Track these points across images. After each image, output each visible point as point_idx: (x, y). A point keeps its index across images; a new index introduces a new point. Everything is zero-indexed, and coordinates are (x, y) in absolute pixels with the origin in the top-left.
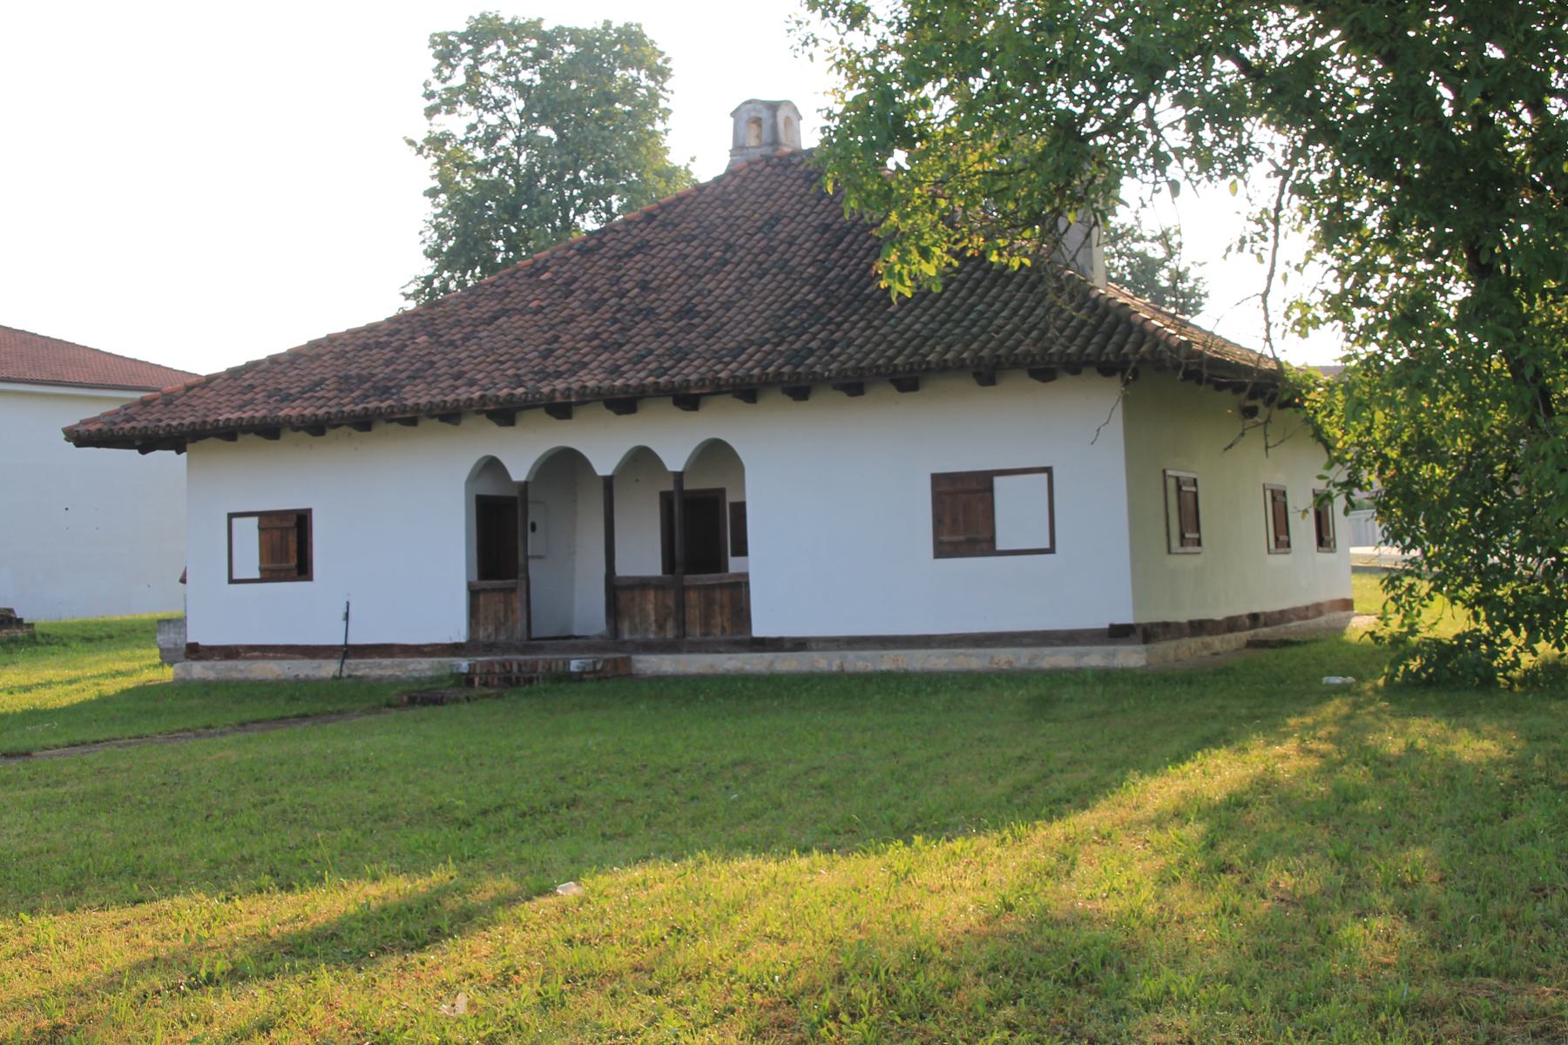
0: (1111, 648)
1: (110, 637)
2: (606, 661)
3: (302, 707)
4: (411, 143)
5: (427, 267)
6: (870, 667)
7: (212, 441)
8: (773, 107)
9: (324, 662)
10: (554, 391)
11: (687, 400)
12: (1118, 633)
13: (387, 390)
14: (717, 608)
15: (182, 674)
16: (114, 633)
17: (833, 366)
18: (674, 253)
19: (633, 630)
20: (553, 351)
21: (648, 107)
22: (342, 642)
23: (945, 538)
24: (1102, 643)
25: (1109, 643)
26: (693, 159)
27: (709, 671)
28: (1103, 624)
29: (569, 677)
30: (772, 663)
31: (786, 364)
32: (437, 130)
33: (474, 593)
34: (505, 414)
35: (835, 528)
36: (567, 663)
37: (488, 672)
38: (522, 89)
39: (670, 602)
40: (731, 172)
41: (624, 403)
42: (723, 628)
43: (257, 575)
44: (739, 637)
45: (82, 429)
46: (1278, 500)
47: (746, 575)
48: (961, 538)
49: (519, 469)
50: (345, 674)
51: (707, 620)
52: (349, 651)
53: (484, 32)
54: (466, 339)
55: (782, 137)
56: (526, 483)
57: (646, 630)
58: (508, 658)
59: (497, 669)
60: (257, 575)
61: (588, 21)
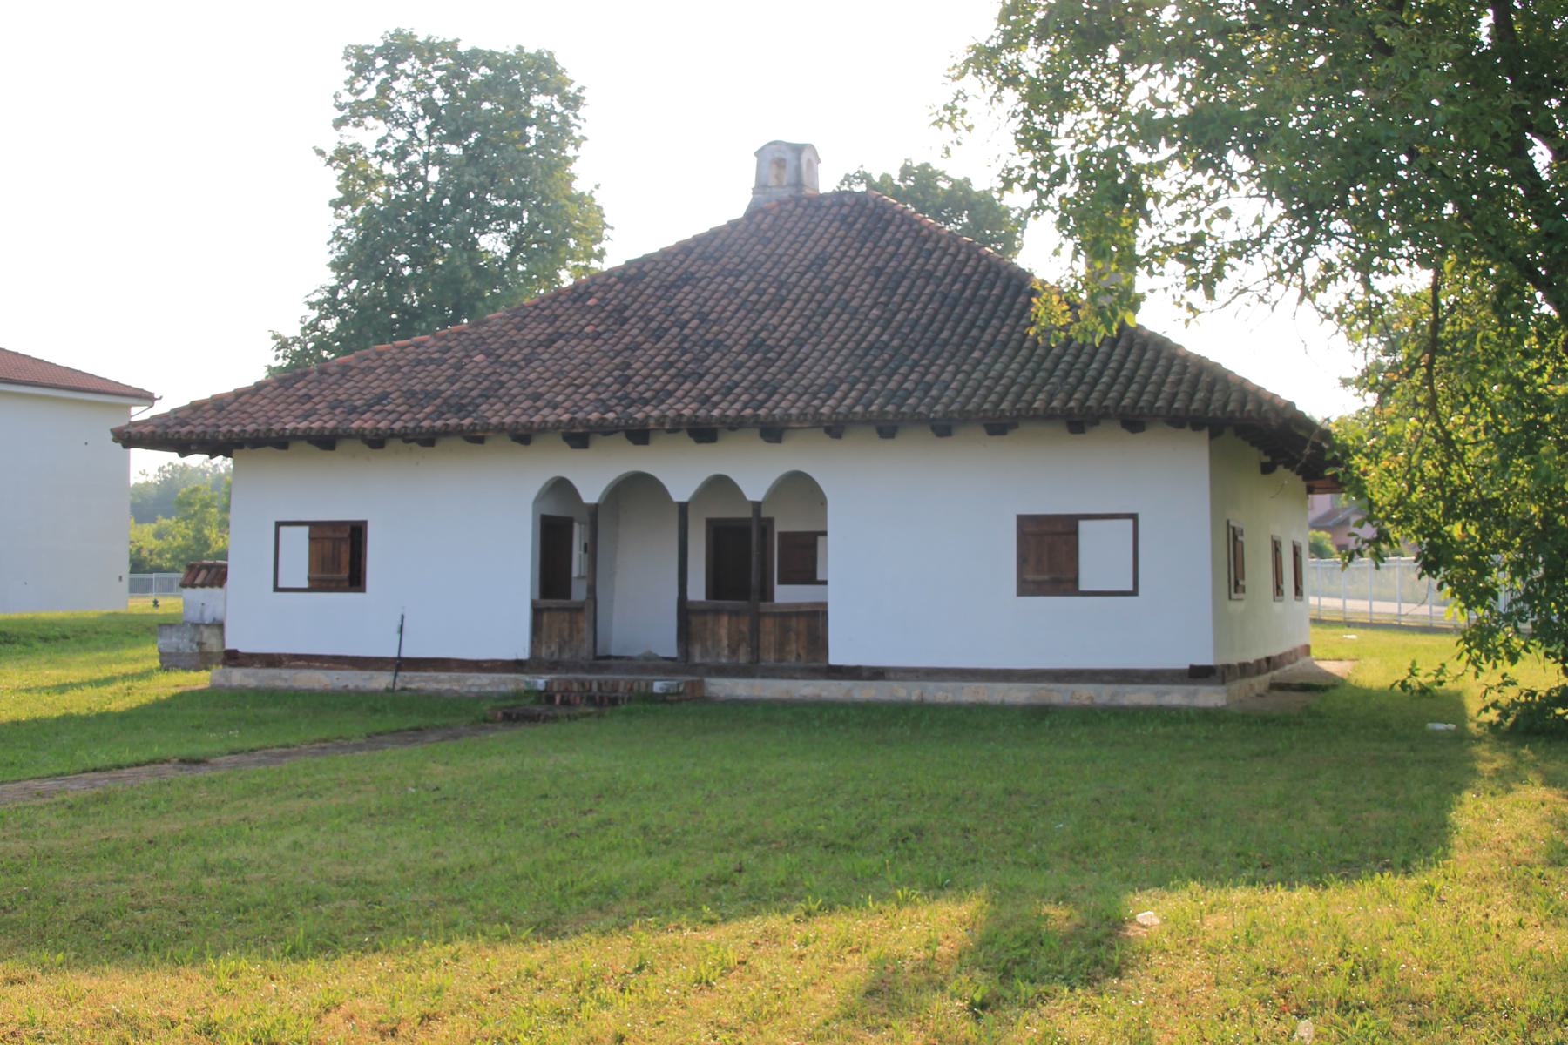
0: (1192, 688)
1: (66, 637)
2: (687, 683)
3: (416, 720)
4: (321, 153)
5: (330, 279)
6: (950, 698)
7: (269, 449)
8: (798, 149)
9: (375, 674)
10: (648, 417)
11: (773, 432)
12: (1199, 674)
13: (461, 408)
14: (793, 636)
15: (222, 681)
16: (69, 633)
17: (938, 408)
18: (724, 287)
19: (705, 652)
20: (629, 378)
21: (558, 135)
22: (394, 654)
23: (1030, 577)
24: (1182, 682)
25: (1188, 683)
26: (597, 187)
27: (785, 696)
28: (1183, 664)
29: (651, 698)
30: (850, 690)
31: (888, 403)
32: (348, 142)
33: (537, 612)
34: (578, 438)
35: (914, 563)
36: (649, 684)
37: (566, 690)
38: (429, 107)
39: (745, 628)
40: (751, 214)
41: (704, 433)
42: (799, 655)
43: (305, 585)
44: (815, 665)
45: (133, 430)
46: (1277, 547)
47: (825, 605)
48: (1046, 577)
49: (591, 491)
50: (398, 687)
51: (781, 647)
52: (402, 664)
53: (399, 48)
54: (528, 360)
55: (805, 179)
56: (596, 505)
57: (718, 654)
58: (569, 680)
59: (575, 687)
60: (305, 585)
61: (501, 42)
